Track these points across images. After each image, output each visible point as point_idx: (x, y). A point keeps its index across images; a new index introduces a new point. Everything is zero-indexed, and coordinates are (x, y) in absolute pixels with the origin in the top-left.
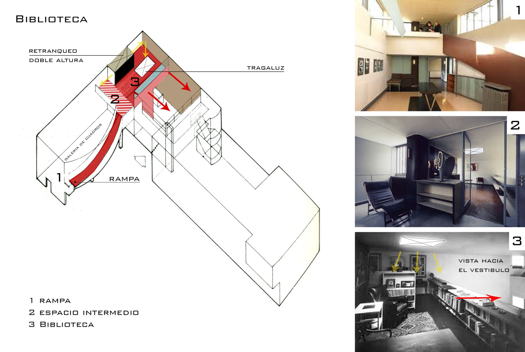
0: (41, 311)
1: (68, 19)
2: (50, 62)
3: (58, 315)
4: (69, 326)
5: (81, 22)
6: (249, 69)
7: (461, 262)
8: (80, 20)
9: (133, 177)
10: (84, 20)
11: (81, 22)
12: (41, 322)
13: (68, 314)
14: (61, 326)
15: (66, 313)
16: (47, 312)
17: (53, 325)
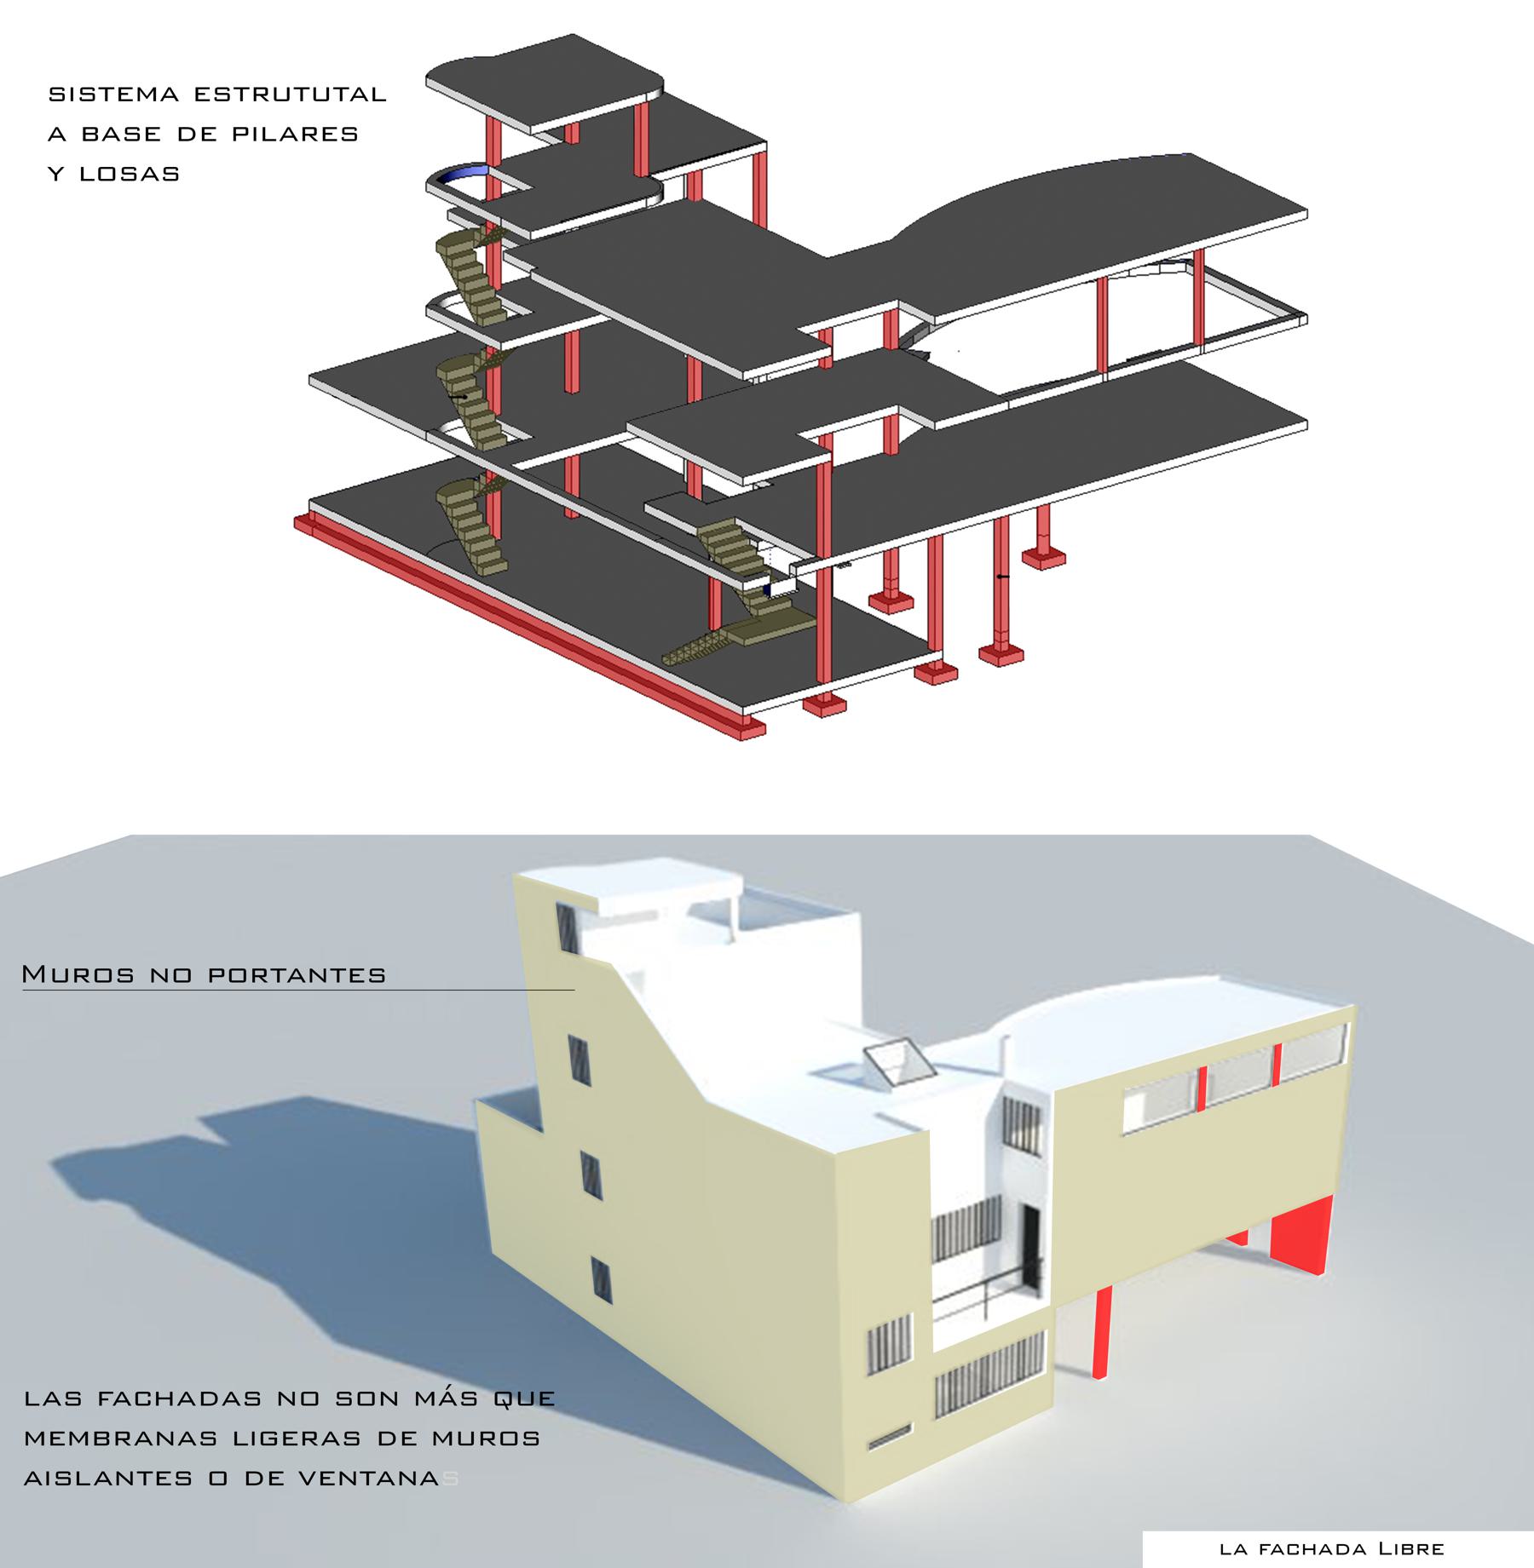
0: (197, 89)
1: (358, 975)
4: (225, 1483)
5: (104, 140)
7: (307, 1484)
11: (104, 140)
15: (143, 1399)
17: (64, 1478)
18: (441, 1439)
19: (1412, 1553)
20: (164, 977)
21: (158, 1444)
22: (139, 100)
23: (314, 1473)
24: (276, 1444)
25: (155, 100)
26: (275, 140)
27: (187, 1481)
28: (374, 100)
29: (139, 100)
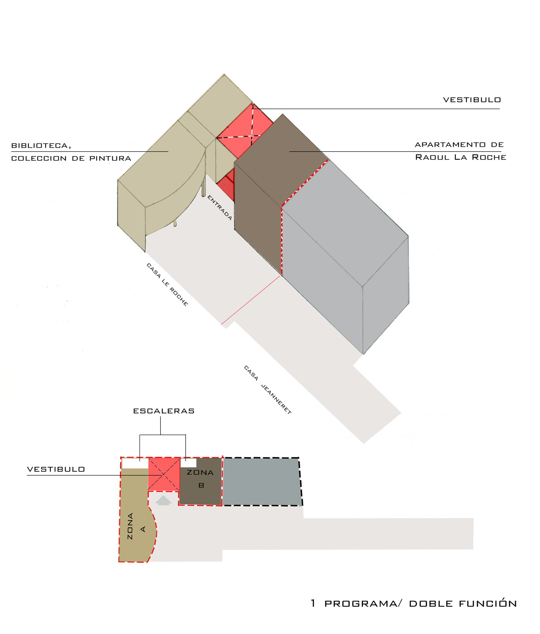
2: (32, 160)
3: (428, 147)
6: (455, 155)
7: (446, 102)
8: (154, 411)
9: (426, 143)
10: (256, 378)
12: (168, 409)
13: (492, 159)
14: (33, 147)
15: (490, 604)
16: (43, 468)
18: (455, 145)
19: (435, 606)
20: (514, 604)
21: (467, 147)
22: (380, 606)
23: (449, 98)
24: (359, 606)
25: (387, 606)
26: (459, 159)
27: (144, 412)
28: (162, 413)
29: (380, 606)
